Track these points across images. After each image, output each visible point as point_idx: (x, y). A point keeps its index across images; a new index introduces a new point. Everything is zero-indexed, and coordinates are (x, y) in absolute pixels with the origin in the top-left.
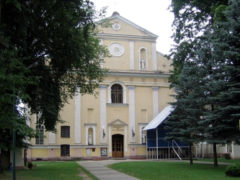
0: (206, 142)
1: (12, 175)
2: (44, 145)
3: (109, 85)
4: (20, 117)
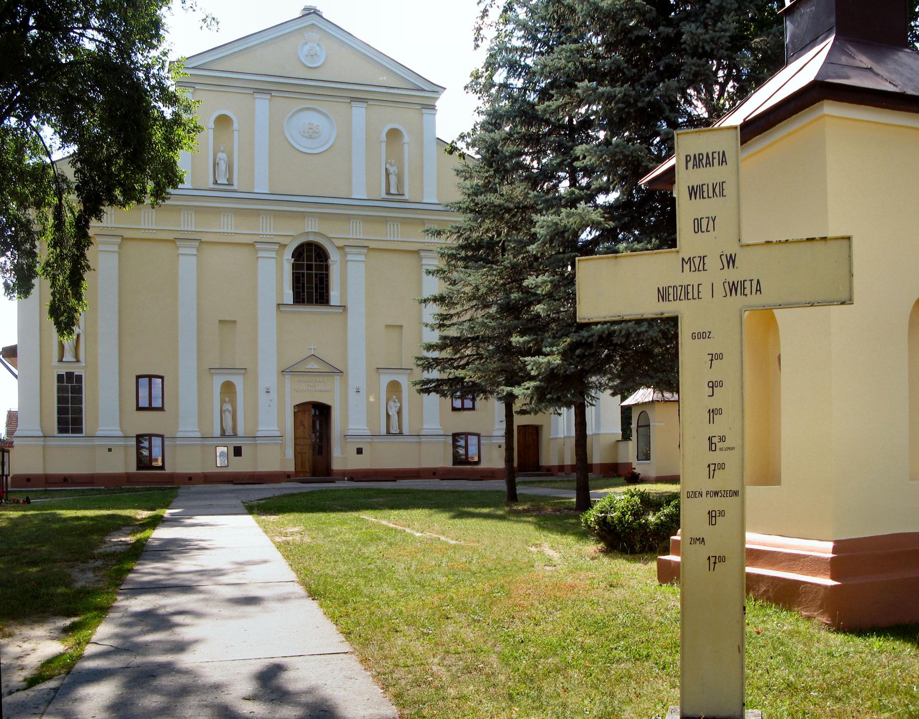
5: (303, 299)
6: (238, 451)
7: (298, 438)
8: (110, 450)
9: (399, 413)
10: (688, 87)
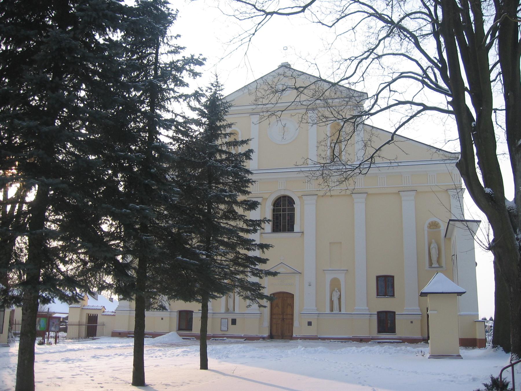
5: (280, 229)
6: (234, 322)
7: (292, 315)
8: (162, 319)
9: (339, 299)
10: (220, 176)
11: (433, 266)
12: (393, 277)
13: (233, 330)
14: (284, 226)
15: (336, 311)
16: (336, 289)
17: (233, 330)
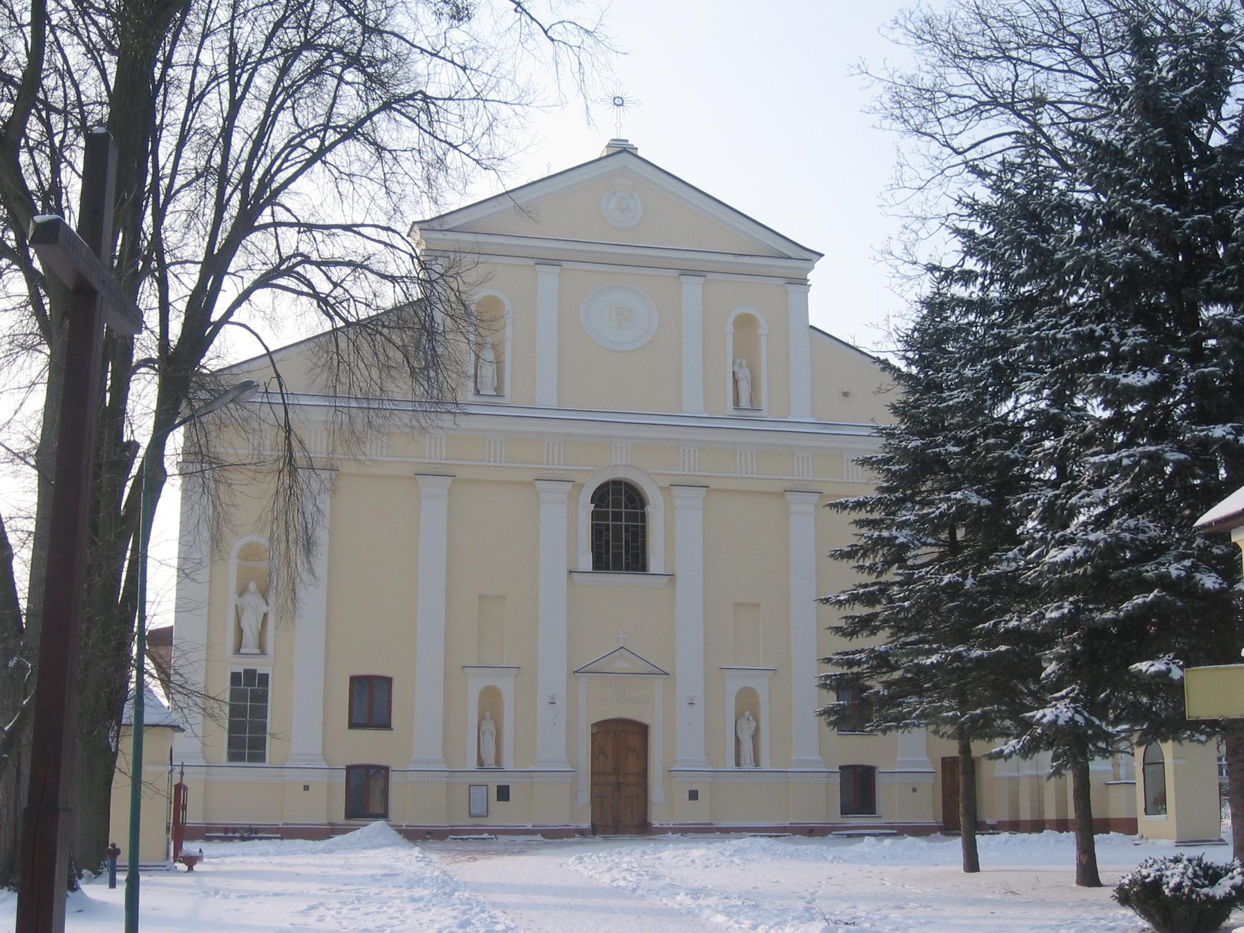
0: (1050, 754)
1: (118, 896)
2: (267, 764)
3: (582, 486)
4: (1097, 382)
6: (503, 793)
8: (306, 788)
9: (755, 737)
11: (242, 651)
12: (388, 681)
13: (501, 815)
14: (617, 557)
15: (748, 764)
16: (747, 713)
17: (501, 815)
